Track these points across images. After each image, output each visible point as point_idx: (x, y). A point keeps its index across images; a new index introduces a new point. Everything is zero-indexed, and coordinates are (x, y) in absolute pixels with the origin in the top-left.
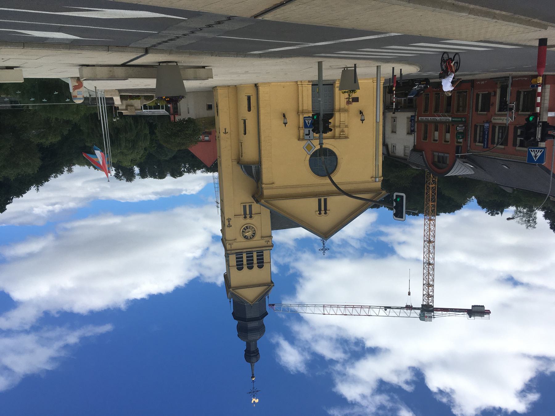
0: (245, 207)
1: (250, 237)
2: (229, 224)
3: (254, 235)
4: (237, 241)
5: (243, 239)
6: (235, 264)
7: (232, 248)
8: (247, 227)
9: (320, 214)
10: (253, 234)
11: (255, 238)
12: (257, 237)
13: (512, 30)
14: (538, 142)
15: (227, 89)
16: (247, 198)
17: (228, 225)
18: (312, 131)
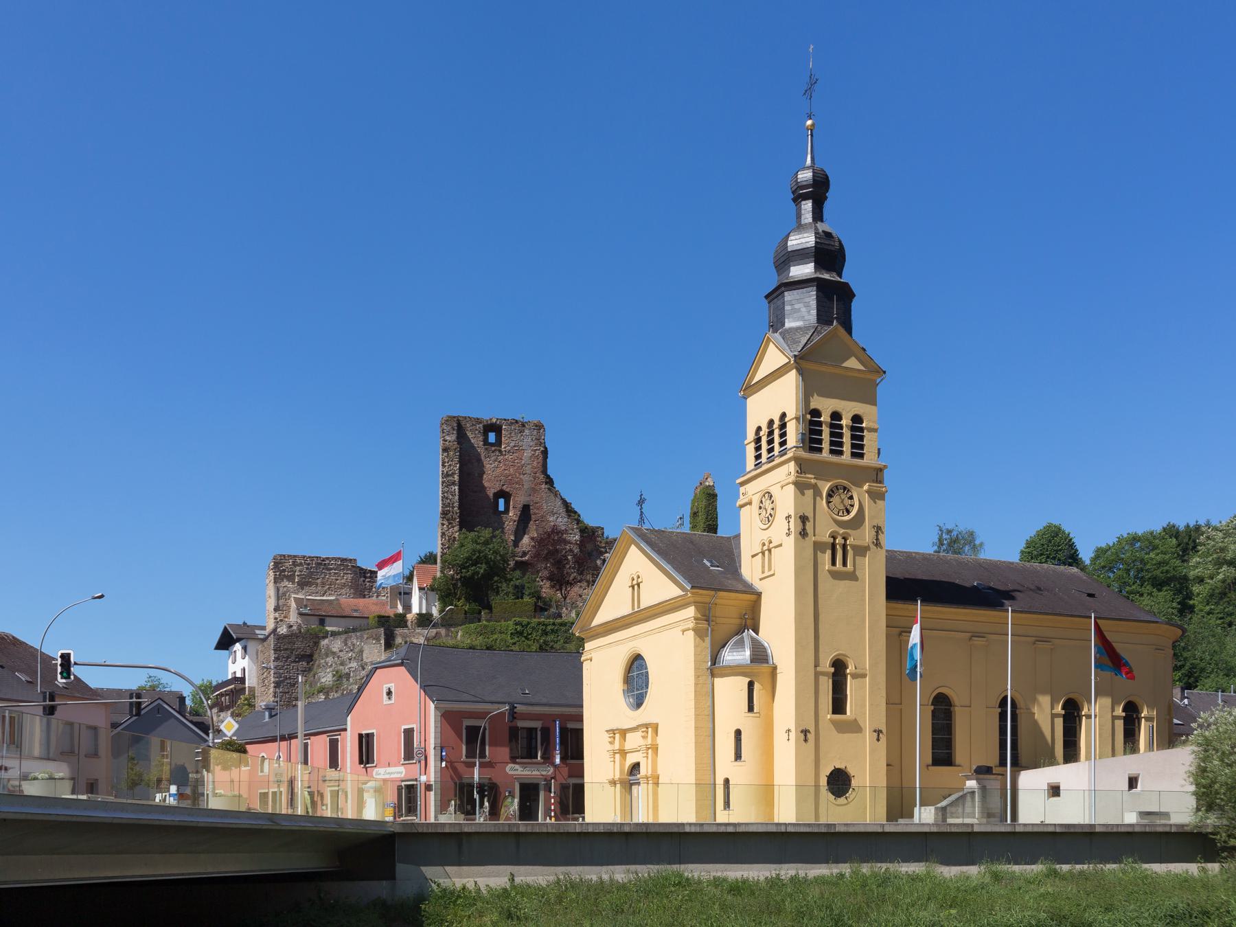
0: (770, 569)
4: (779, 485)
5: (772, 490)
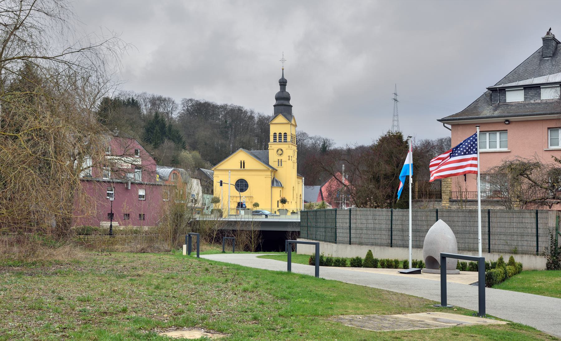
0: (281, 165)
5: (282, 149)
6: (287, 137)
9: (244, 161)
11: (277, 149)
16: (280, 170)
18: (384, 140)
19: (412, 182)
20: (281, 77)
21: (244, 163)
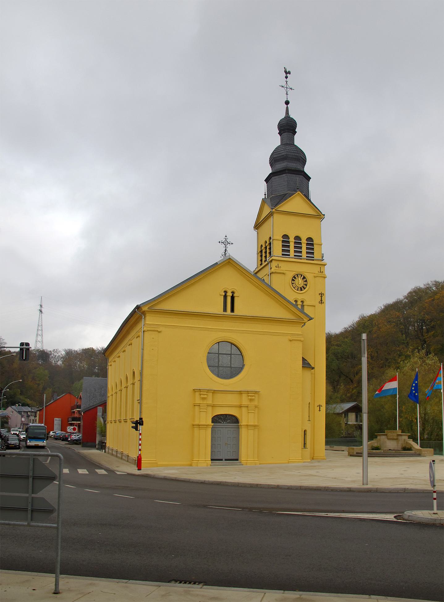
1: (298, 276)
2: (321, 297)
3: (293, 279)
7: (319, 267)
8: (301, 290)
9: (233, 293)
10: (295, 279)
11: (291, 275)
12: (290, 275)
13: (6, 549)
14: (429, 431)
15: (315, 456)
17: (322, 296)
19: (363, 359)
20: (283, 116)
21: (233, 298)
